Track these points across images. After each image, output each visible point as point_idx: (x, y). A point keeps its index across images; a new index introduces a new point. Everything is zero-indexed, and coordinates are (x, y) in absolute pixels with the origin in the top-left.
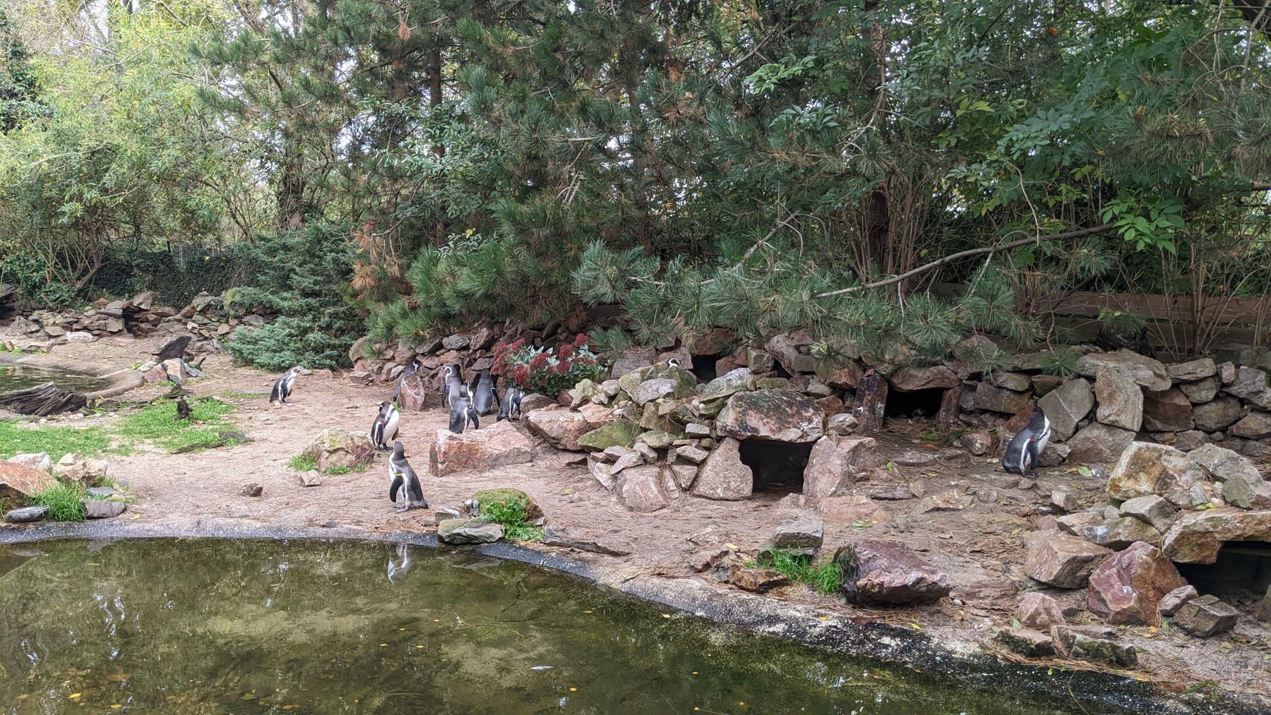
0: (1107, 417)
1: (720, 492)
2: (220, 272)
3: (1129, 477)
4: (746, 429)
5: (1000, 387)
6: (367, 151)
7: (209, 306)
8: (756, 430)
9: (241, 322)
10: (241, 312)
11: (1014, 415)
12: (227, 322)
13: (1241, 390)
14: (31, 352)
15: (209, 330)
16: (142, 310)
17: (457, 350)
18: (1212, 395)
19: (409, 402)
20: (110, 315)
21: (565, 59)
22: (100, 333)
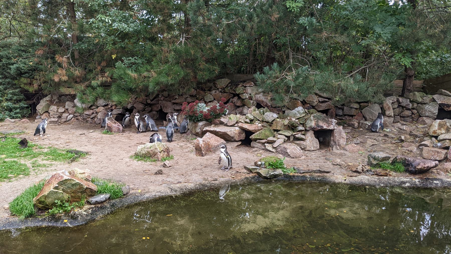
0: (389, 114)
1: (312, 149)
3: (439, 129)
4: (319, 127)
5: (351, 108)
8: (322, 127)
11: (355, 116)
13: (404, 104)
17: (103, 106)
18: (397, 106)
19: (114, 129)
21: (320, 21)
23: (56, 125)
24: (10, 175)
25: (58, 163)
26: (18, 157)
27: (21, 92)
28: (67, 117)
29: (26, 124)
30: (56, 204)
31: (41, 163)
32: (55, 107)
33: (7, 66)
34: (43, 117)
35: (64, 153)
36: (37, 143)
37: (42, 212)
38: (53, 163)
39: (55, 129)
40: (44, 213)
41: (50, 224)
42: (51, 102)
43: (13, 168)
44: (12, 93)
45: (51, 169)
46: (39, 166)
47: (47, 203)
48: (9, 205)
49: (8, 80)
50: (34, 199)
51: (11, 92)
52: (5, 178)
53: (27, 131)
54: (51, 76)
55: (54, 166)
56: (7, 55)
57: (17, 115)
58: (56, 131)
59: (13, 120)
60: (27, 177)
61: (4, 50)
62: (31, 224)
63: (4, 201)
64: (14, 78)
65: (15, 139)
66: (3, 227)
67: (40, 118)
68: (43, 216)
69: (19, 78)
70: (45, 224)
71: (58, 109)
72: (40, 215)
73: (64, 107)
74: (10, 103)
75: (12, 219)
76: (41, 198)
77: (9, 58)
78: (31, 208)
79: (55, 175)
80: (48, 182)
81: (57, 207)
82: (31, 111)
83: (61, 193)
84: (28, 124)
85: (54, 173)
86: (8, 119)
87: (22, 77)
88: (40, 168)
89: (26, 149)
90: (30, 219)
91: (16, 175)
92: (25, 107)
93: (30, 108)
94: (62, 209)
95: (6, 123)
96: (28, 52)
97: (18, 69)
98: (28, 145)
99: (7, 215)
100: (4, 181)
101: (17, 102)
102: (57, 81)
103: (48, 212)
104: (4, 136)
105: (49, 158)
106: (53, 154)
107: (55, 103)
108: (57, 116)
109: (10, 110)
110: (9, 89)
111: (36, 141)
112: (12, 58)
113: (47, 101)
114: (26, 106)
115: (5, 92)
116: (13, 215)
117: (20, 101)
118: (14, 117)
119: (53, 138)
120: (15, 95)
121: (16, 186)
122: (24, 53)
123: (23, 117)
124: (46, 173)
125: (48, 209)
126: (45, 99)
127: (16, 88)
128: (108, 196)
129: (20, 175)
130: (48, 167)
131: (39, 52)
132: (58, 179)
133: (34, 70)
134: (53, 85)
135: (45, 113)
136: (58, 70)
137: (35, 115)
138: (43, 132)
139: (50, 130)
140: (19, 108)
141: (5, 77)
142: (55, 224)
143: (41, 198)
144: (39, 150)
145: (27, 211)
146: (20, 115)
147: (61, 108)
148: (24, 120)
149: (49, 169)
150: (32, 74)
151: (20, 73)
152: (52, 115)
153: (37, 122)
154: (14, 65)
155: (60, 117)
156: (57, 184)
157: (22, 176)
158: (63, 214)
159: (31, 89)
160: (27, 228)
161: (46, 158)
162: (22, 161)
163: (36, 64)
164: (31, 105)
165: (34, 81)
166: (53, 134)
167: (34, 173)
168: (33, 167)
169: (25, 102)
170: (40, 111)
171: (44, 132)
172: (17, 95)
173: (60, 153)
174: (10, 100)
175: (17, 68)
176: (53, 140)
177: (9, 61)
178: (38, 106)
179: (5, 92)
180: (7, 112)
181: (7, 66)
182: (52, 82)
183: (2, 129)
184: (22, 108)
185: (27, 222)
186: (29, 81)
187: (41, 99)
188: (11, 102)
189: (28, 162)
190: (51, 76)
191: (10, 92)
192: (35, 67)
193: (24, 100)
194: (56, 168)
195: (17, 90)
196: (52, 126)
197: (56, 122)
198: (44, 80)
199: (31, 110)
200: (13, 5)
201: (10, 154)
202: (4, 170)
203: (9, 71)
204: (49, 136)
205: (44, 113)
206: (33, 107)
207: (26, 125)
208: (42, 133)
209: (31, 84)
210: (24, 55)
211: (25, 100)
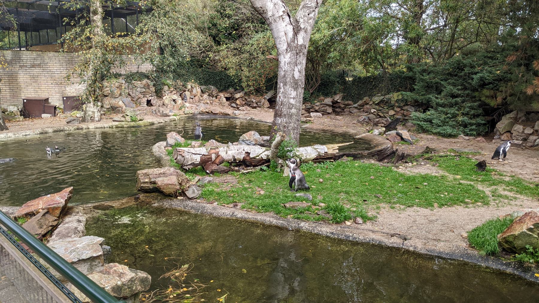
2: (371, 84)
6: (86, 15)
7: (382, 101)
9: (402, 109)
10: (402, 105)
12: (393, 109)
14: (307, 123)
15: (383, 113)
16: (338, 102)
20: (327, 105)
22: (325, 113)
23: (519, 149)
24: (467, 200)
25: (525, 198)
26: (474, 181)
27: (480, 106)
28: (535, 140)
29: (481, 144)
30: (527, 249)
31: (503, 193)
32: (521, 127)
33: (469, 76)
34: (503, 137)
35: (531, 186)
36: (496, 168)
37: (506, 254)
38: (517, 196)
39: (517, 153)
40: (508, 256)
41: (516, 272)
42: (516, 120)
43: (470, 193)
44: (470, 107)
45: (516, 203)
46: (500, 196)
47: (515, 245)
48: (467, 234)
49: (467, 92)
50: (499, 236)
51: (469, 105)
52: (461, 202)
53: (483, 152)
54: (523, 87)
55: (518, 200)
56: (470, 63)
57: (472, 132)
58: (519, 157)
59: (467, 138)
60: (486, 206)
61: (468, 58)
62: (493, 265)
63: (461, 228)
64: (474, 90)
65: (470, 160)
66: (461, 257)
67: (500, 138)
68: (508, 259)
69: (481, 90)
70: (509, 270)
71: (524, 129)
72: (504, 257)
73: (533, 127)
74: (466, 118)
75: (470, 251)
76: (508, 237)
77: (472, 67)
78: (495, 246)
79: (529, 213)
80: (520, 220)
81: (527, 253)
82: (488, 129)
83: (535, 237)
84: (483, 144)
85: (530, 210)
86: (462, 135)
87: (484, 88)
88: (502, 200)
89: (484, 173)
90: (492, 258)
91: (473, 201)
92: (481, 124)
93: (488, 125)
94: (533, 258)
95: (459, 140)
96: (495, 59)
97: (482, 79)
98: (486, 169)
99: (465, 244)
100: (461, 205)
101: (474, 117)
102: (530, 94)
103: (515, 257)
104: (458, 154)
105: (512, 189)
106: (517, 185)
107: (520, 121)
108: (522, 138)
109: (465, 126)
110: (467, 101)
111: (495, 165)
112: (476, 66)
113: (511, 118)
114: (483, 122)
115: (462, 105)
116: (472, 247)
117: (478, 116)
118: (468, 134)
119: (516, 165)
120: (473, 109)
121: (474, 214)
122: (490, 60)
123: (479, 135)
124: (509, 207)
125: (515, 253)
126: (508, 116)
127: (475, 102)
128: (81, 193)
129: (478, 202)
130: (511, 200)
131: (511, 58)
132: (534, 219)
133: (500, 79)
134: (522, 98)
135: (507, 133)
136: (535, 80)
137: (491, 134)
138: (503, 156)
139: (512, 155)
140: (475, 124)
141: (464, 88)
142: (522, 275)
143: (508, 237)
144: (498, 176)
145: (489, 248)
146: (475, 133)
147: (528, 128)
148: (479, 139)
149: (513, 203)
150: (497, 85)
151: (483, 84)
152: (515, 136)
153: (494, 143)
154: (478, 74)
155: (525, 140)
156: (533, 225)
157: (480, 204)
158: (533, 266)
159: (493, 103)
160: (487, 268)
161: (508, 188)
162: (480, 187)
163: (504, 73)
164: (488, 122)
165: (498, 94)
166: (516, 160)
167: (494, 204)
168: (493, 196)
169: (483, 118)
170: (500, 130)
171: (505, 156)
172: (475, 109)
173: (527, 186)
174: (467, 114)
175: (481, 77)
176: (515, 167)
177: (473, 71)
178: (498, 123)
179: (462, 105)
180: (462, 128)
181: (469, 76)
182: (521, 96)
183: (455, 146)
184: (478, 125)
185: (487, 260)
186: (492, 92)
187: (503, 115)
188: (467, 117)
189: (487, 190)
190: (523, 87)
191: (467, 105)
192: (502, 76)
193: (482, 116)
194: (521, 203)
195: (476, 104)
196: (513, 150)
197: (520, 145)
198: (511, 92)
199: (488, 127)
200: (489, 4)
201: (466, 176)
202: (460, 192)
203: (470, 81)
204: (511, 162)
205: (505, 132)
206: (492, 124)
207: (482, 145)
208: (501, 157)
209: (494, 97)
210: (490, 62)
211: (483, 116)
